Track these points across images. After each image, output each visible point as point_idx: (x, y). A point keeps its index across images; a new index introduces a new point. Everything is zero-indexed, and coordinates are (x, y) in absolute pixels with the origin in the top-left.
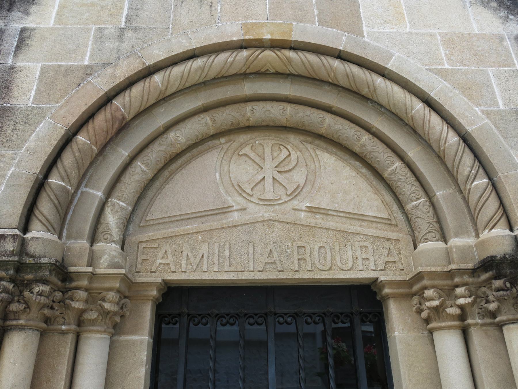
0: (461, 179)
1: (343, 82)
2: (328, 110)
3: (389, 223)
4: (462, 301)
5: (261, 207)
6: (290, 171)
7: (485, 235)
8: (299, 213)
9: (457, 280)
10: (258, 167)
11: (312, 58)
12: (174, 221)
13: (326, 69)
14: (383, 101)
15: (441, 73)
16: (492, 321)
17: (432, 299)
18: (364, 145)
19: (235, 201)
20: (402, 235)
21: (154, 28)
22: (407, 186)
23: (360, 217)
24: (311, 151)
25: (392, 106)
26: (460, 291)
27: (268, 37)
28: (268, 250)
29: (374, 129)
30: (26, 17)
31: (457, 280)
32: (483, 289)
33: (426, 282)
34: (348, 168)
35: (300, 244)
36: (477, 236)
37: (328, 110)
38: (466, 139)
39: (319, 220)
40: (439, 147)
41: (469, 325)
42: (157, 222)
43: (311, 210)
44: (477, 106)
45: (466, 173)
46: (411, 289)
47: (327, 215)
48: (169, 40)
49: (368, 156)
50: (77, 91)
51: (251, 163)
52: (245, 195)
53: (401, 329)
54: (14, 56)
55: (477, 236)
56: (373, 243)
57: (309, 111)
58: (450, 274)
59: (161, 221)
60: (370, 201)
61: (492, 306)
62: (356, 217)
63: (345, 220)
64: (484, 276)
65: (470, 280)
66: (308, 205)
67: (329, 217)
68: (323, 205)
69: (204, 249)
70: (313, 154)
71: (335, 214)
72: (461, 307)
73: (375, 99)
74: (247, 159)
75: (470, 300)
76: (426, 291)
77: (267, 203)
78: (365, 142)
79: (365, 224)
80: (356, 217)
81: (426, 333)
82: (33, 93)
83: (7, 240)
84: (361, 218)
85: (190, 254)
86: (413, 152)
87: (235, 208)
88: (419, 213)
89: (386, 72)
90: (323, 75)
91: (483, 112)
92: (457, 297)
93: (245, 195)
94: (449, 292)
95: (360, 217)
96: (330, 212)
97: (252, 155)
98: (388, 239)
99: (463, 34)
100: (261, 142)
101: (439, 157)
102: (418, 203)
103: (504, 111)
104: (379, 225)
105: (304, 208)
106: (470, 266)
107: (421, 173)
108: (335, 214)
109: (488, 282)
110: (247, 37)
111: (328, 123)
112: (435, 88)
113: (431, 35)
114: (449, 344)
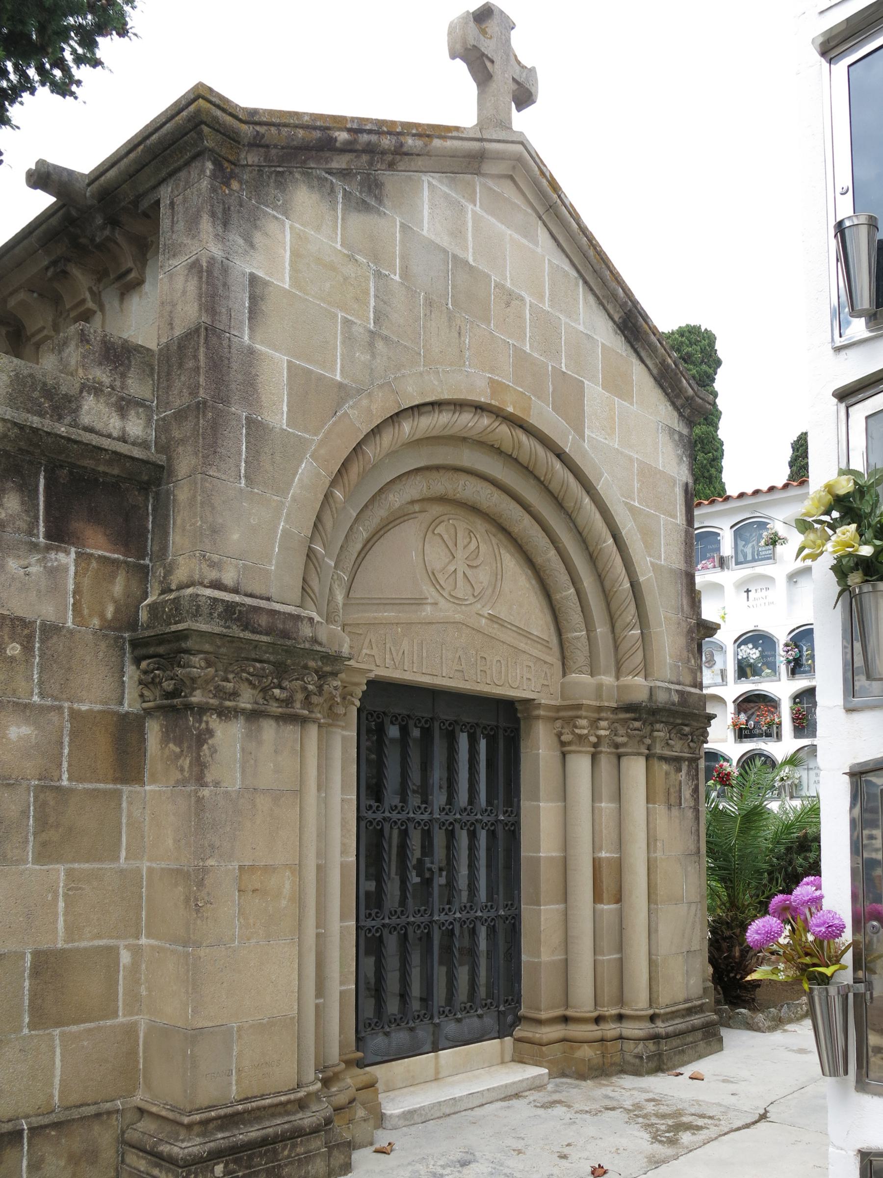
0: (619, 625)
1: (554, 486)
2: (526, 507)
3: (546, 644)
4: (602, 733)
5: (451, 605)
6: (476, 567)
7: (627, 680)
8: (481, 618)
9: (603, 715)
10: (449, 554)
11: (540, 450)
12: (373, 604)
13: (547, 469)
14: (580, 521)
15: (632, 509)
16: (614, 750)
17: (584, 728)
18: (549, 560)
19: (429, 591)
20: (554, 658)
21: (405, 346)
22: (575, 617)
23: (527, 635)
24: (495, 547)
25: (586, 530)
26: (603, 724)
27: (510, 409)
28: (457, 656)
29: (560, 545)
30: (252, 252)
31: (603, 715)
32: (616, 724)
33: (583, 713)
34: (524, 577)
35: (483, 654)
36: (618, 678)
37: (526, 507)
38: (635, 585)
39: (494, 629)
40: (613, 586)
41: (601, 752)
42: (358, 602)
43: (493, 618)
44: (650, 556)
45: (628, 620)
46: (566, 714)
47: (503, 626)
48: (421, 374)
49: (547, 572)
50: (335, 423)
51: (444, 547)
52: (438, 587)
53: (540, 747)
54: (250, 328)
55: (618, 678)
56: (535, 664)
57: (513, 505)
58: (600, 709)
59: (361, 602)
60: (538, 622)
61: (620, 740)
62: (524, 633)
63: (515, 635)
64: (623, 716)
65: (611, 716)
66: (490, 612)
67: (503, 629)
68: (502, 616)
69: (405, 645)
70: (496, 551)
71: (509, 626)
72: (598, 737)
73: (574, 515)
74: (440, 541)
75: (607, 733)
76: (579, 720)
77: (457, 601)
78: (549, 556)
79: (529, 642)
80: (524, 633)
81: (558, 753)
82: (285, 409)
83: (304, 622)
84: (525, 634)
85: (392, 648)
86: (588, 582)
87: (429, 601)
88: (579, 645)
89: (593, 492)
90: (541, 472)
91: (651, 562)
92: (597, 728)
93: (438, 587)
94: (594, 724)
95: (527, 635)
96: (506, 624)
97: (446, 537)
98: (545, 662)
99: (652, 466)
100: (455, 522)
101: (607, 596)
102: (577, 634)
103: (664, 566)
104: (539, 646)
105: (486, 615)
106: (614, 705)
107: (590, 605)
108: (509, 626)
109: (625, 721)
110: (493, 402)
111: (524, 525)
112: (628, 527)
113: (631, 459)
114: (581, 765)
